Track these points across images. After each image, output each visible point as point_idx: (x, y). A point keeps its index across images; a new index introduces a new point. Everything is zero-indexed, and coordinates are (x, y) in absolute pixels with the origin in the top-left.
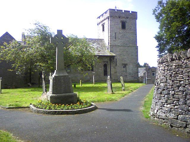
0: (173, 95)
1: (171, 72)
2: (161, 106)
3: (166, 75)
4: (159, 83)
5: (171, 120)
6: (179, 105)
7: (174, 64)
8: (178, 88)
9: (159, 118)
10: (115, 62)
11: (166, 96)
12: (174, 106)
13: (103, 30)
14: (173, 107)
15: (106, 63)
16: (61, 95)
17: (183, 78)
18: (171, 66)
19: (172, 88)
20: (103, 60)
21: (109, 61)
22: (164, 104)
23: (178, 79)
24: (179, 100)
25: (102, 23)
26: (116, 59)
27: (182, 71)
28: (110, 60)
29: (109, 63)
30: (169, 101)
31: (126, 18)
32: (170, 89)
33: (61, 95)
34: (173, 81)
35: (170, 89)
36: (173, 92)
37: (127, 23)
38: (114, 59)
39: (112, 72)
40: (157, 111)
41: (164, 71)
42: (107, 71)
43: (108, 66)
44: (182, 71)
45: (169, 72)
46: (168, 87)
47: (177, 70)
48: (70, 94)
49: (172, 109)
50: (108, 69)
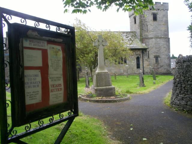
0: (184, 88)
1: (183, 70)
2: (177, 96)
3: (180, 72)
4: (176, 78)
5: (183, 106)
6: (188, 94)
7: (185, 65)
8: (188, 82)
9: (176, 104)
10: (147, 54)
11: (180, 88)
12: (185, 95)
13: (135, 23)
14: (184, 96)
15: (139, 56)
16: (103, 87)
17: (191, 75)
18: (184, 66)
19: (184, 82)
20: (136, 53)
21: (141, 54)
22: (179, 94)
23: (187, 76)
24: (187, 91)
25: (134, 16)
26: (148, 52)
27: (190, 70)
28: (143, 53)
29: (141, 56)
30: (182, 92)
31: (157, 9)
32: (182, 83)
33: (103, 87)
34: (184, 77)
35: (182, 83)
36: (184, 85)
37: (158, 14)
38: (146, 52)
39: (144, 65)
40: (174, 99)
41: (179, 69)
42: (139, 64)
43: (140, 59)
44: (190, 70)
45: (182, 70)
46: (181, 81)
47: (187, 69)
48: (110, 87)
49: (184, 98)
50: (140, 62)
